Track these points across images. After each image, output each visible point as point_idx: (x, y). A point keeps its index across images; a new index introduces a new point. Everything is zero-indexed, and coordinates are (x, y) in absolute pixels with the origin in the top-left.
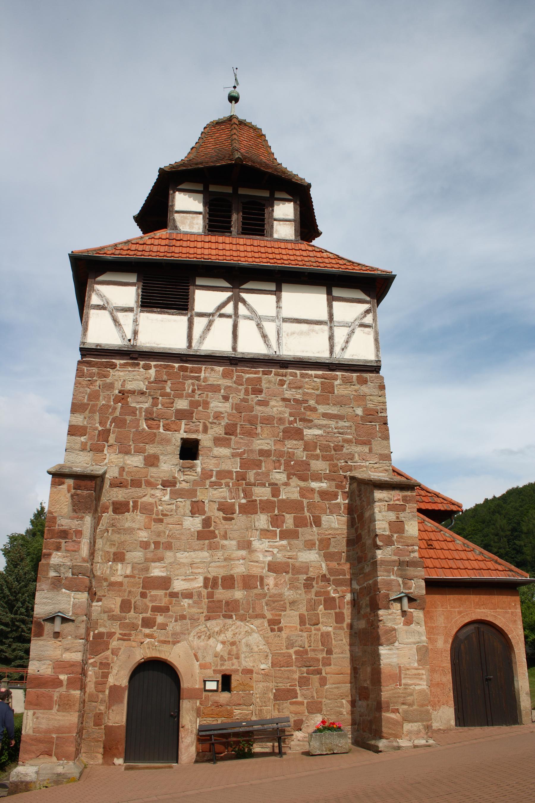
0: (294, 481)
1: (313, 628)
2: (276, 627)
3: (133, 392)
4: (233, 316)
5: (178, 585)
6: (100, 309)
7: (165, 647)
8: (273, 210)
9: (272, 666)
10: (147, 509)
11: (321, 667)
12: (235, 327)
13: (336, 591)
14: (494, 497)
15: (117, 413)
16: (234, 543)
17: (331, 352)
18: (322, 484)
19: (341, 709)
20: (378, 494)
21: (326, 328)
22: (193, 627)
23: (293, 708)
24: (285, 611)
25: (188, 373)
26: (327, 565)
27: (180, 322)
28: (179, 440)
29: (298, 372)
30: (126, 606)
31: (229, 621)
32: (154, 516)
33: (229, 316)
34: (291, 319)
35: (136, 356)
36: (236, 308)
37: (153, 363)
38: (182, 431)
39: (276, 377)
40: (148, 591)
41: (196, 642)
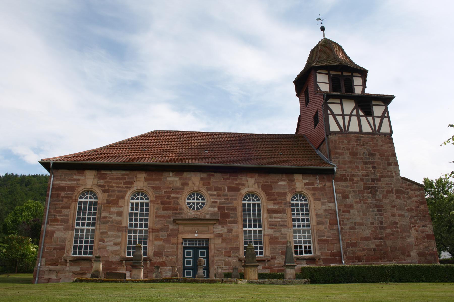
14: (6, 174)
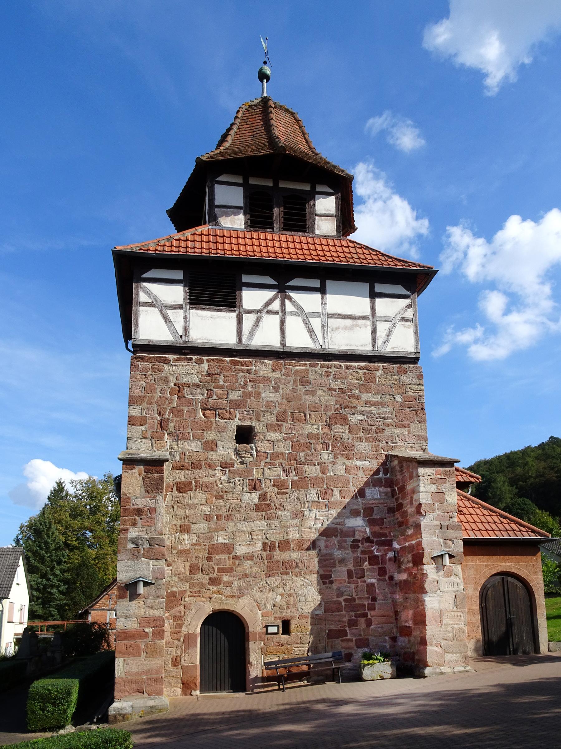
0: (341, 460)
1: (359, 580)
2: (327, 581)
3: (188, 385)
4: (280, 313)
5: (241, 550)
6: (149, 306)
7: (231, 601)
8: (314, 205)
9: (325, 612)
10: (208, 488)
11: (367, 611)
12: (283, 322)
13: (378, 550)
15: (175, 405)
16: (288, 513)
17: (374, 346)
18: (366, 462)
19: (385, 644)
20: (422, 471)
21: (369, 323)
22: (255, 584)
23: (344, 644)
24: (335, 567)
25: (240, 367)
26: (370, 529)
27: (230, 318)
28: (235, 427)
29: (342, 364)
30: (193, 569)
31: (286, 577)
32: (215, 493)
33: (277, 313)
34: (336, 314)
35: (189, 352)
36: (283, 304)
37: (205, 358)
38: (237, 420)
39: (322, 369)
40: (213, 556)
41: (258, 595)
